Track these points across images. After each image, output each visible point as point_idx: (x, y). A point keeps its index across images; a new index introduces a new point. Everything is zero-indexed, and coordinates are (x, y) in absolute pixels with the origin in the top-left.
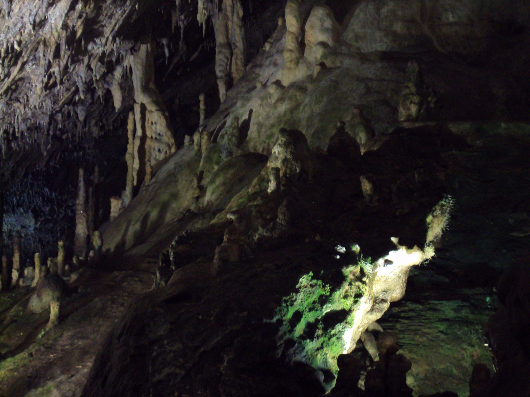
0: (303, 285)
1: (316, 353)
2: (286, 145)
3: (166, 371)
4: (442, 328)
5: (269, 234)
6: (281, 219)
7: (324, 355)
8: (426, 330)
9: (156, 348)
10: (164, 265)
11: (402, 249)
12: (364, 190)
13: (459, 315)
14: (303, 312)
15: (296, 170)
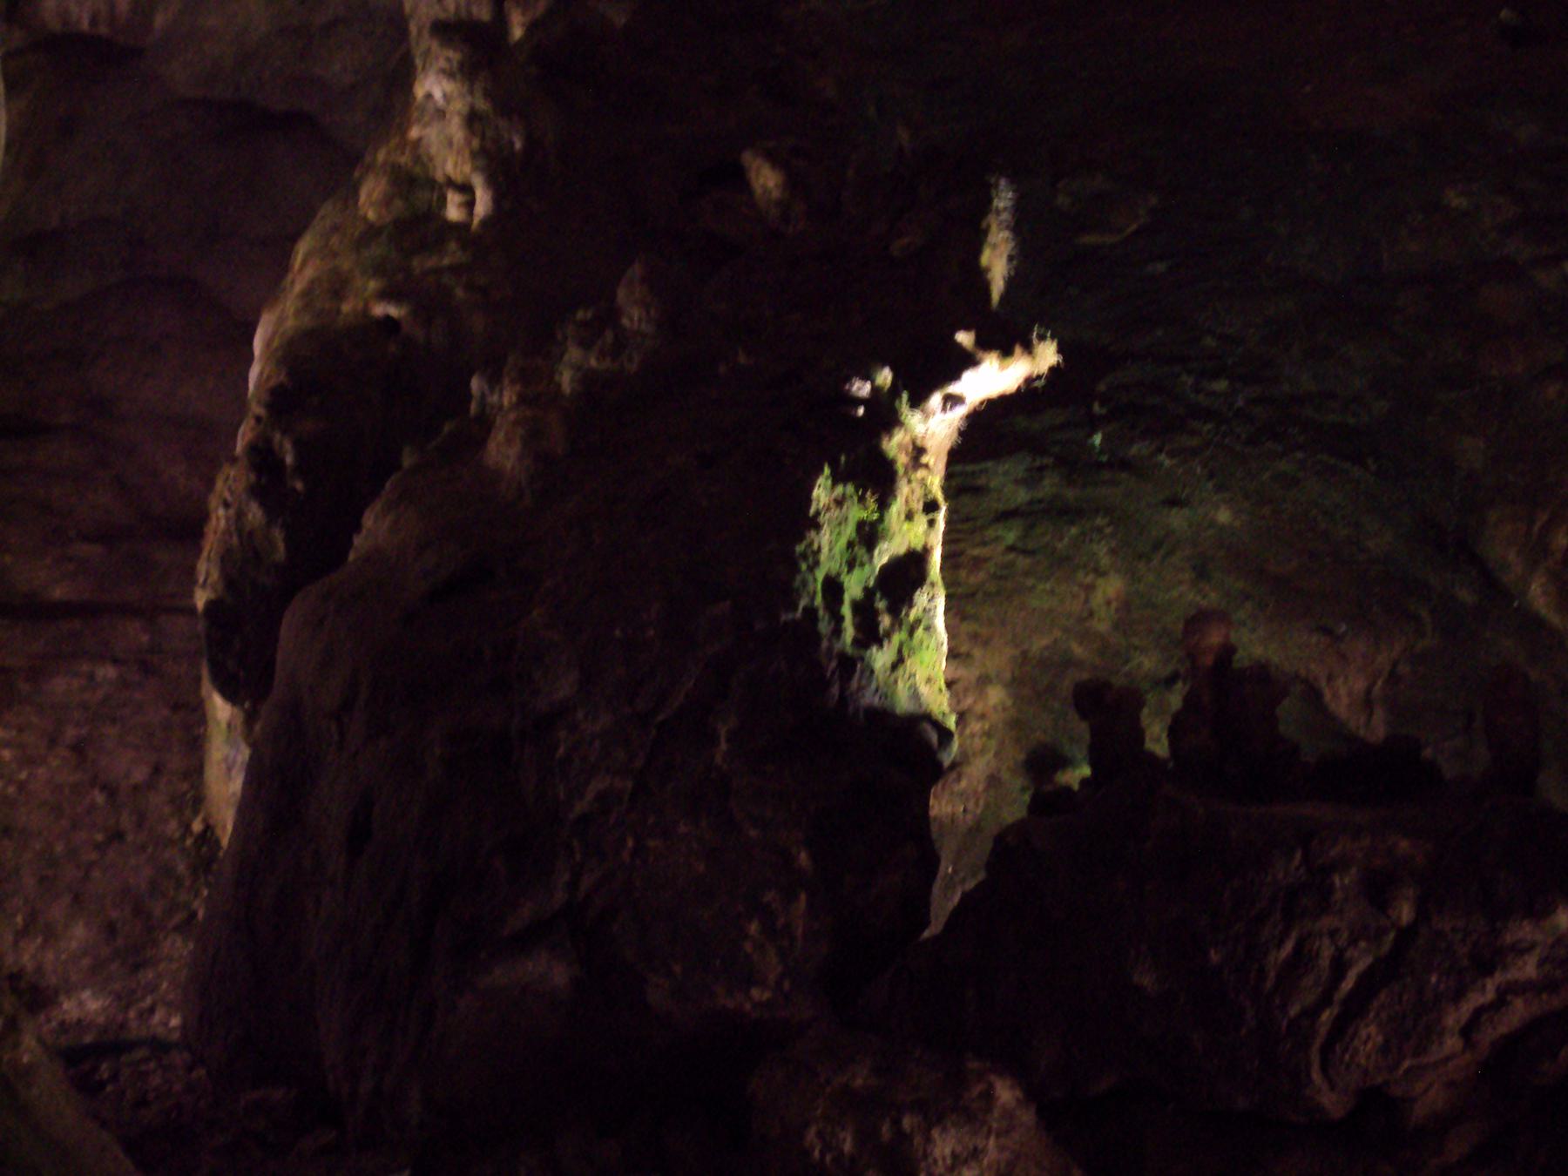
0: (821, 505)
1: (892, 678)
2: (467, 72)
3: (596, 786)
4: (1011, 537)
5: (607, 364)
6: (634, 317)
7: (909, 678)
8: (976, 552)
9: (562, 734)
10: (263, 481)
11: (991, 363)
12: (758, 191)
13: (1040, 495)
14: (839, 575)
15: (512, 143)
